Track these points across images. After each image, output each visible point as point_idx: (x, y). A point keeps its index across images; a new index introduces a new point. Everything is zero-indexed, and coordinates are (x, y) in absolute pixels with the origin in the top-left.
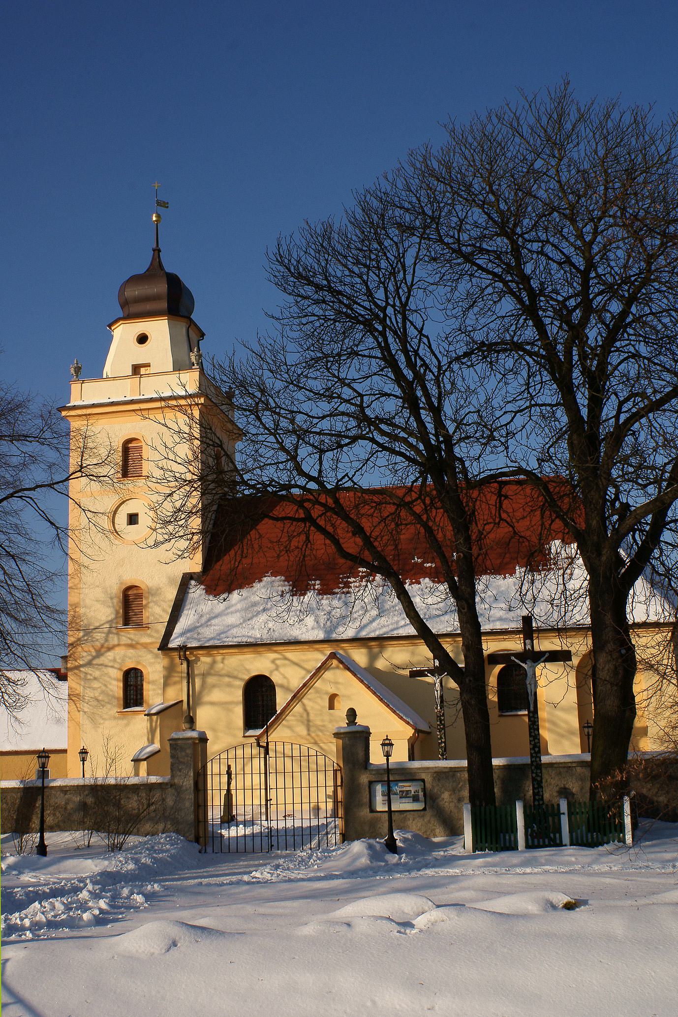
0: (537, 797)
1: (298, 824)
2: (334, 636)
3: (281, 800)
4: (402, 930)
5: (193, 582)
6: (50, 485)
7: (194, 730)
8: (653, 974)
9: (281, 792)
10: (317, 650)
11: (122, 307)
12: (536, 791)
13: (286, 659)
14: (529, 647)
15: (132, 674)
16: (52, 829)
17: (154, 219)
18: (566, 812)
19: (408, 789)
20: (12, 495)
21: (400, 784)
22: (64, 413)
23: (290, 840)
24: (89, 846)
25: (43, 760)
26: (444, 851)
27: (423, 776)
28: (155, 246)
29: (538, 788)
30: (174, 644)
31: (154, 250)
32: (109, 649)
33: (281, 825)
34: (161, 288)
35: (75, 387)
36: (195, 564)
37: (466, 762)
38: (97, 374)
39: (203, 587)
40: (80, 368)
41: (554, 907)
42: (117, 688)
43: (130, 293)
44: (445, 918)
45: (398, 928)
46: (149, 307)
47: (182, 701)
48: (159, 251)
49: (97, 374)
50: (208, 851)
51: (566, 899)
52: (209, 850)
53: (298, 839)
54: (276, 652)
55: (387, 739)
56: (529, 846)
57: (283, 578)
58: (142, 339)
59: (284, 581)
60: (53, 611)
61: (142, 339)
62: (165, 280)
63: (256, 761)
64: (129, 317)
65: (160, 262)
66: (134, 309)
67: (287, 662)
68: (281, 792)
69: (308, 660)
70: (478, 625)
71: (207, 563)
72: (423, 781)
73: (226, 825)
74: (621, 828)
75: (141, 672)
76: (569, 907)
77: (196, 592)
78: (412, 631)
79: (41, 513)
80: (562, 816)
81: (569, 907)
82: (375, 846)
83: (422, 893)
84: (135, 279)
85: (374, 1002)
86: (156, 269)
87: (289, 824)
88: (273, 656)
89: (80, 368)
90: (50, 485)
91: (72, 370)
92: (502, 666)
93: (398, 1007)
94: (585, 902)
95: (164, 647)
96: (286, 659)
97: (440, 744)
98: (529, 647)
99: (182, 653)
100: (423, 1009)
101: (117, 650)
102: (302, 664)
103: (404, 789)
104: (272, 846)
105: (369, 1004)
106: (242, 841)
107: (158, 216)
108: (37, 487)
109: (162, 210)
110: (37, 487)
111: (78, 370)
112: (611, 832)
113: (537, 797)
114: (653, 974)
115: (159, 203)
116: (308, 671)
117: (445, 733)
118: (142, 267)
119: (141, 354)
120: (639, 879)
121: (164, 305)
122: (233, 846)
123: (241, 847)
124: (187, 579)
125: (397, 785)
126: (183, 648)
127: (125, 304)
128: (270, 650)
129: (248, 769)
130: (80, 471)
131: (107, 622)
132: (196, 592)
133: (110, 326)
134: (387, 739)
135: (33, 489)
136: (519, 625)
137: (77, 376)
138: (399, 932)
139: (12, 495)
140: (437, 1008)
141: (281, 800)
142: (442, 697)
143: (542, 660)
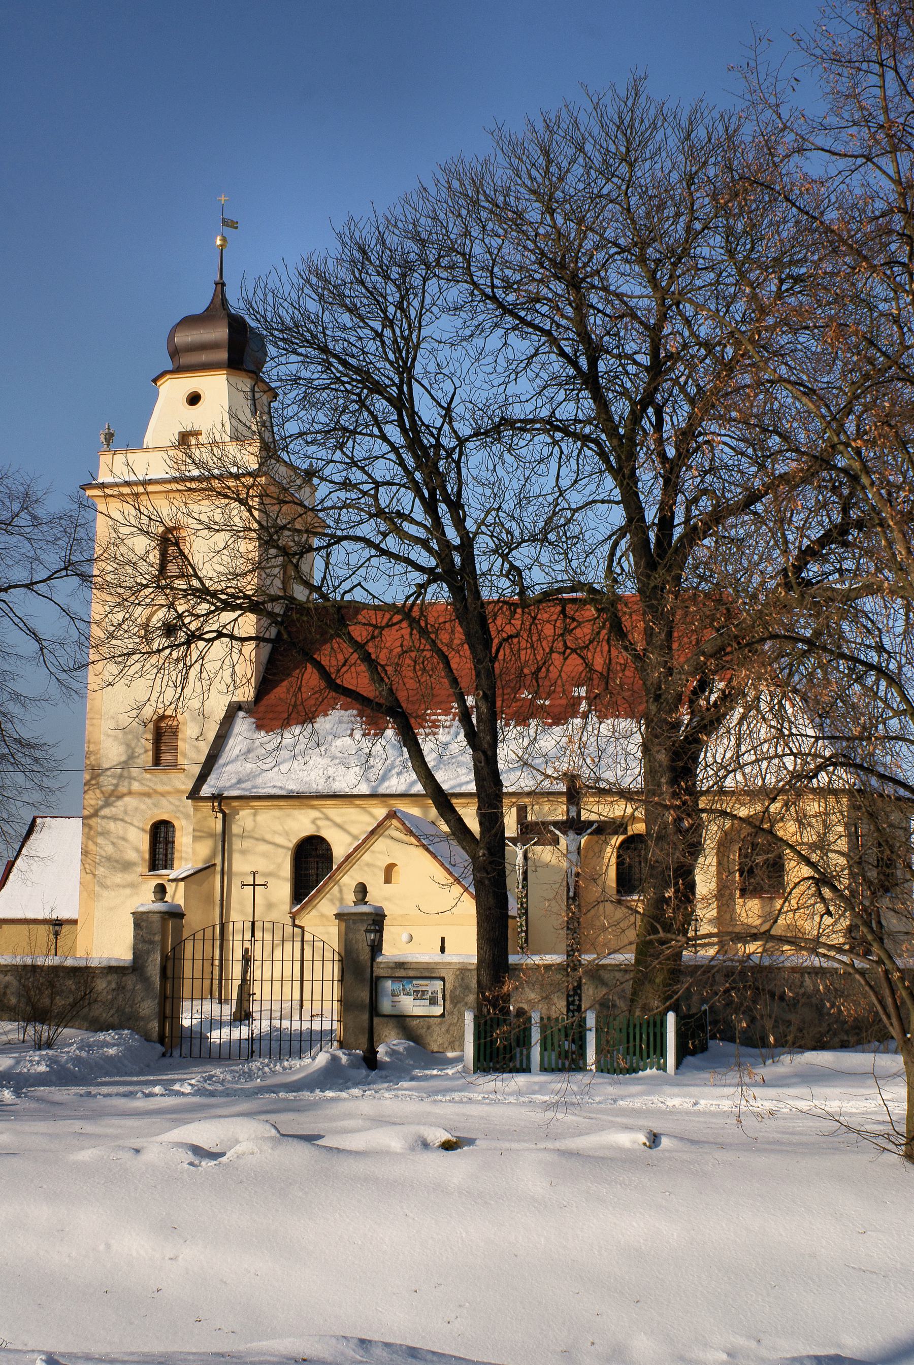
0: (571, 1007)
2: (382, 790)
4: (197, 1162)
6: (26, 586)
7: (366, 903)
8: (464, 1235)
10: (358, 806)
13: (328, 818)
14: (573, 814)
17: (219, 242)
19: (424, 988)
21: (415, 982)
22: (89, 493)
23: (295, 1045)
25: (57, 928)
26: (441, 1070)
27: (443, 974)
28: (218, 279)
29: (573, 996)
31: (216, 284)
32: (120, 797)
33: (306, 1025)
34: (220, 333)
35: (105, 459)
36: (246, 694)
38: (135, 443)
39: (253, 720)
41: (425, 1145)
42: (143, 842)
43: (184, 338)
44: (256, 1150)
45: (190, 1157)
46: (204, 357)
48: (223, 285)
49: (135, 443)
51: (445, 1136)
52: (176, 1053)
57: (355, 712)
58: (194, 399)
59: (355, 716)
60: (34, 748)
61: (194, 399)
63: (288, 946)
64: (179, 369)
66: (185, 360)
69: (353, 822)
70: (499, 784)
72: (443, 979)
73: (238, 1023)
75: (173, 826)
76: (448, 1146)
77: (243, 725)
78: (419, 788)
79: (16, 620)
81: (448, 1146)
82: (340, 1059)
83: (264, 1117)
84: (190, 321)
85: (108, 1246)
87: (316, 1026)
88: (314, 814)
89: (112, 435)
90: (26, 586)
91: (102, 438)
92: (478, 836)
93: (134, 1254)
94: (470, 1142)
95: (194, 794)
96: (328, 818)
97: (519, 933)
98: (573, 814)
100: (163, 1258)
101: (127, 799)
102: (347, 827)
103: (420, 988)
104: (253, 1052)
105: (102, 1247)
106: (245, 1045)
107: (224, 239)
108: (10, 587)
109: (228, 231)
110: (10, 587)
111: (109, 437)
112: (648, 1057)
113: (571, 1007)
114: (464, 1235)
115: (226, 223)
118: (199, 306)
119: (193, 418)
120: (604, 1117)
121: (223, 355)
123: (225, 1051)
126: (218, 798)
127: (175, 352)
128: (352, 803)
129: (278, 954)
130: (66, 568)
131: (120, 763)
132: (243, 725)
133: (155, 381)
136: (562, 787)
138: (191, 1164)
140: (180, 1258)
141: (267, 996)
143: (589, 831)
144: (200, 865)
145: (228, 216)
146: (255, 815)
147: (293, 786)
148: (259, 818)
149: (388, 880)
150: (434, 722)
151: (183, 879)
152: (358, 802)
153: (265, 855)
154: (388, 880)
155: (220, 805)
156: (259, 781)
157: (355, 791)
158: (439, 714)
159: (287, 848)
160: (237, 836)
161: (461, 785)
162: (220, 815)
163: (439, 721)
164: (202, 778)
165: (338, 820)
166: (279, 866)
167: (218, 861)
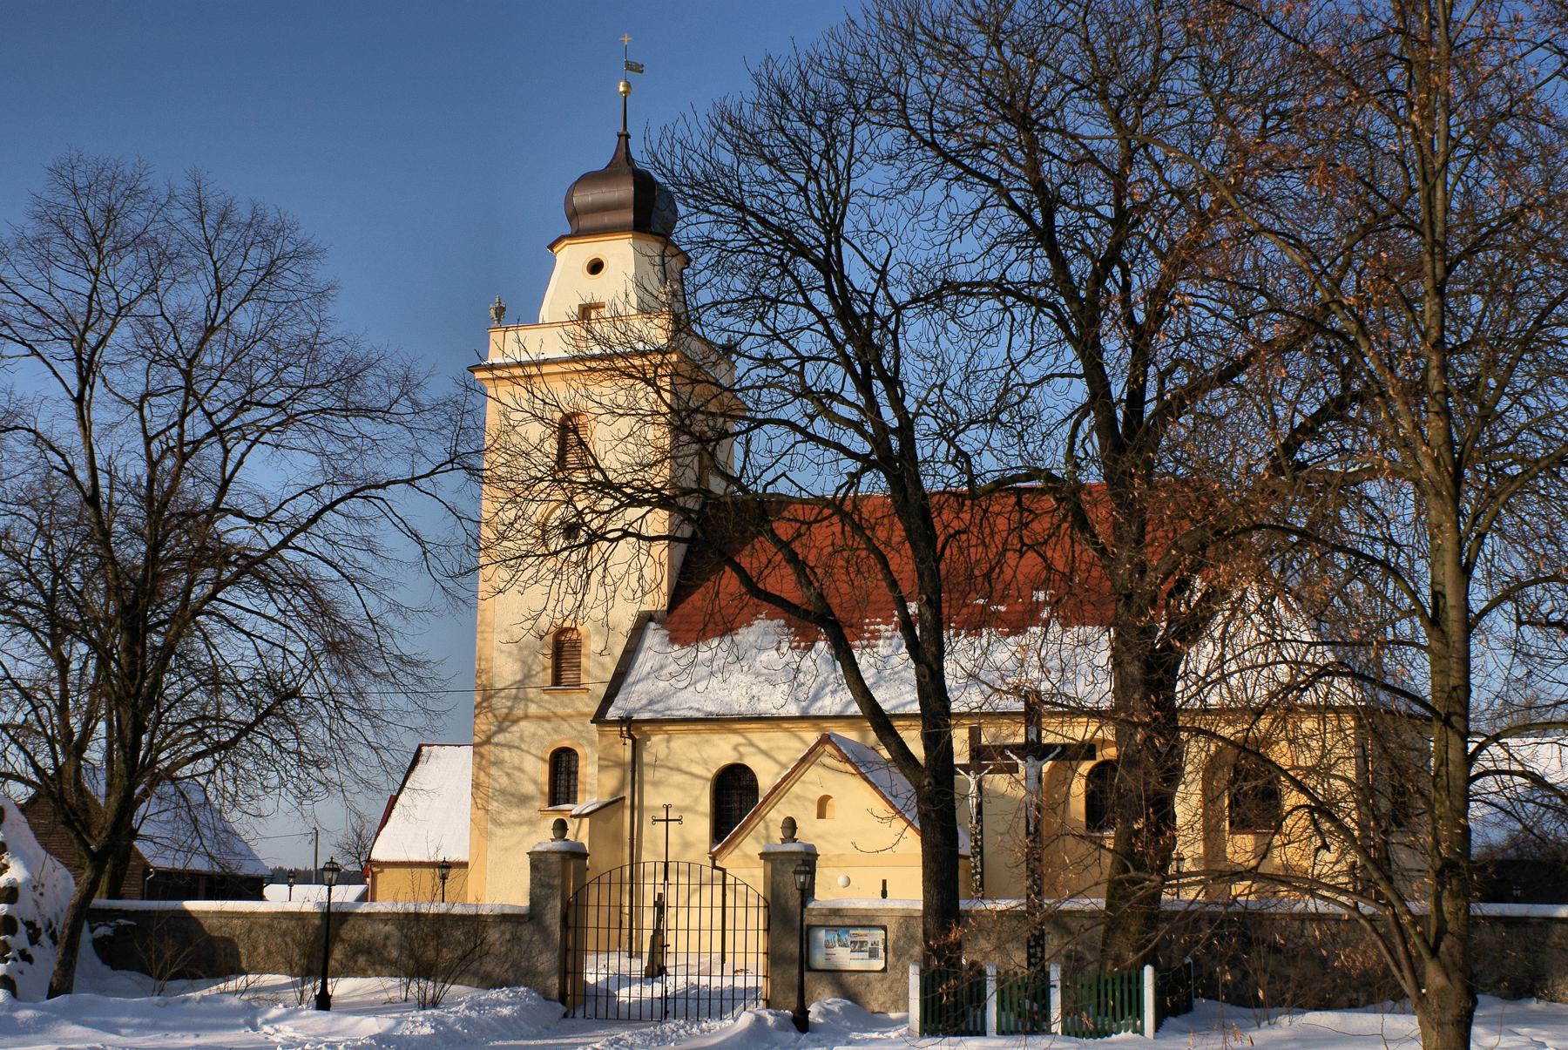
0: (1033, 960)
1: (716, 982)
2: (813, 711)
3: (682, 948)
5: (652, 625)
7: (795, 841)
9: (682, 936)
10: (786, 730)
11: (570, 219)
12: (1032, 951)
13: (752, 744)
14: (1033, 736)
15: (564, 758)
16: (337, 974)
17: (622, 89)
18: (1059, 984)
20: (351, 495)
21: (852, 932)
22: (478, 375)
24: (406, 1000)
25: (444, 871)
27: (884, 922)
29: (1035, 947)
30: (613, 713)
31: (620, 136)
34: (624, 191)
35: (496, 336)
36: (657, 601)
37: (961, 907)
39: (666, 632)
40: (504, 309)
43: (583, 198)
46: (607, 219)
47: (624, 798)
48: (628, 136)
50: (577, 1014)
52: (579, 1013)
53: (716, 1004)
54: (735, 731)
55: (332, 862)
56: (1001, 1032)
57: (782, 622)
58: (596, 267)
60: (416, 666)
61: (596, 267)
62: (630, 179)
64: (578, 234)
65: (628, 153)
66: (586, 222)
67: (752, 749)
68: (682, 936)
69: (780, 748)
70: (946, 702)
71: (678, 595)
72: (884, 928)
74: (1139, 1014)
77: (654, 638)
79: (396, 520)
80: (1052, 990)
82: (766, 1020)
84: (590, 179)
86: (622, 163)
89: (504, 309)
90: (407, 482)
91: (492, 312)
95: (599, 718)
96: (752, 744)
97: (973, 875)
99: (624, 729)
102: (774, 754)
103: (858, 939)
107: (628, 85)
108: (389, 483)
109: (632, 75)
110: (389, 483)
111: (500, 311)
113: (1033, 960)
115: (629, 66)
116: (784, 766)
117: (982, 860)
118: (601, 162)
121: (629, 217)
122: (635, 1011)
124: (643, 621)
125: (847, 932)
126: (627, 721)
127: (573, 214)
129: (695, 901)
130: (451, 461)
132: (654, 638)
133: (551, 247)
134: (332, 862)
135: (384, 486)
137: (499, 321)
139: (351, 495)
141: (682, 948)
142: (979, 806)
143: (1051, 756)
144: (606, 799)
145: (635, 58)
146: (668, 741)
147: (712, 708)
148: (673, 744)
149: (821, 814)
150: (872, 632)
151: (587, 815)
152: (786, 725)
153: (680, 787)
154: (821, 814)
155: (629, 730)
156: (673, 702)
157: (783, 713)
158: (879, 624)
159: (707, 779)
160: (649, 765)
161: (904, 705)
162: (629, 742)
163: (879, 631)
164: (608, 700)
165: (764, 746)
166: (697, 800)
167: (627, 793)
